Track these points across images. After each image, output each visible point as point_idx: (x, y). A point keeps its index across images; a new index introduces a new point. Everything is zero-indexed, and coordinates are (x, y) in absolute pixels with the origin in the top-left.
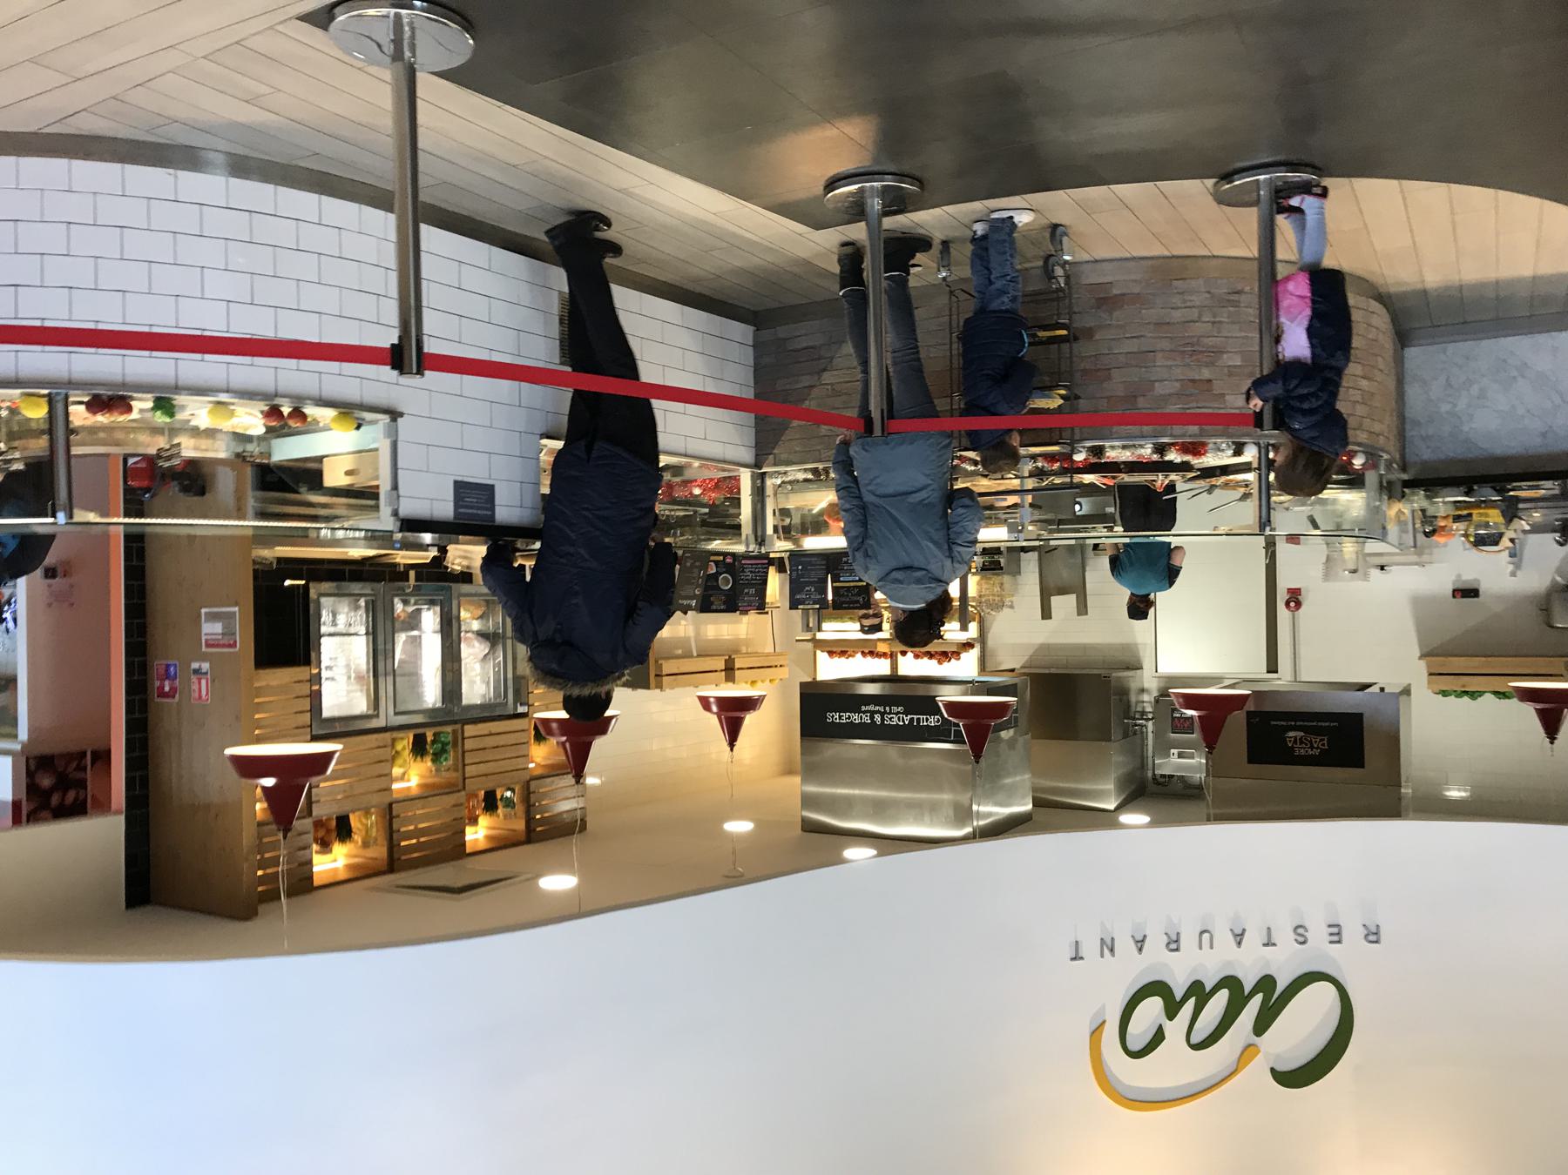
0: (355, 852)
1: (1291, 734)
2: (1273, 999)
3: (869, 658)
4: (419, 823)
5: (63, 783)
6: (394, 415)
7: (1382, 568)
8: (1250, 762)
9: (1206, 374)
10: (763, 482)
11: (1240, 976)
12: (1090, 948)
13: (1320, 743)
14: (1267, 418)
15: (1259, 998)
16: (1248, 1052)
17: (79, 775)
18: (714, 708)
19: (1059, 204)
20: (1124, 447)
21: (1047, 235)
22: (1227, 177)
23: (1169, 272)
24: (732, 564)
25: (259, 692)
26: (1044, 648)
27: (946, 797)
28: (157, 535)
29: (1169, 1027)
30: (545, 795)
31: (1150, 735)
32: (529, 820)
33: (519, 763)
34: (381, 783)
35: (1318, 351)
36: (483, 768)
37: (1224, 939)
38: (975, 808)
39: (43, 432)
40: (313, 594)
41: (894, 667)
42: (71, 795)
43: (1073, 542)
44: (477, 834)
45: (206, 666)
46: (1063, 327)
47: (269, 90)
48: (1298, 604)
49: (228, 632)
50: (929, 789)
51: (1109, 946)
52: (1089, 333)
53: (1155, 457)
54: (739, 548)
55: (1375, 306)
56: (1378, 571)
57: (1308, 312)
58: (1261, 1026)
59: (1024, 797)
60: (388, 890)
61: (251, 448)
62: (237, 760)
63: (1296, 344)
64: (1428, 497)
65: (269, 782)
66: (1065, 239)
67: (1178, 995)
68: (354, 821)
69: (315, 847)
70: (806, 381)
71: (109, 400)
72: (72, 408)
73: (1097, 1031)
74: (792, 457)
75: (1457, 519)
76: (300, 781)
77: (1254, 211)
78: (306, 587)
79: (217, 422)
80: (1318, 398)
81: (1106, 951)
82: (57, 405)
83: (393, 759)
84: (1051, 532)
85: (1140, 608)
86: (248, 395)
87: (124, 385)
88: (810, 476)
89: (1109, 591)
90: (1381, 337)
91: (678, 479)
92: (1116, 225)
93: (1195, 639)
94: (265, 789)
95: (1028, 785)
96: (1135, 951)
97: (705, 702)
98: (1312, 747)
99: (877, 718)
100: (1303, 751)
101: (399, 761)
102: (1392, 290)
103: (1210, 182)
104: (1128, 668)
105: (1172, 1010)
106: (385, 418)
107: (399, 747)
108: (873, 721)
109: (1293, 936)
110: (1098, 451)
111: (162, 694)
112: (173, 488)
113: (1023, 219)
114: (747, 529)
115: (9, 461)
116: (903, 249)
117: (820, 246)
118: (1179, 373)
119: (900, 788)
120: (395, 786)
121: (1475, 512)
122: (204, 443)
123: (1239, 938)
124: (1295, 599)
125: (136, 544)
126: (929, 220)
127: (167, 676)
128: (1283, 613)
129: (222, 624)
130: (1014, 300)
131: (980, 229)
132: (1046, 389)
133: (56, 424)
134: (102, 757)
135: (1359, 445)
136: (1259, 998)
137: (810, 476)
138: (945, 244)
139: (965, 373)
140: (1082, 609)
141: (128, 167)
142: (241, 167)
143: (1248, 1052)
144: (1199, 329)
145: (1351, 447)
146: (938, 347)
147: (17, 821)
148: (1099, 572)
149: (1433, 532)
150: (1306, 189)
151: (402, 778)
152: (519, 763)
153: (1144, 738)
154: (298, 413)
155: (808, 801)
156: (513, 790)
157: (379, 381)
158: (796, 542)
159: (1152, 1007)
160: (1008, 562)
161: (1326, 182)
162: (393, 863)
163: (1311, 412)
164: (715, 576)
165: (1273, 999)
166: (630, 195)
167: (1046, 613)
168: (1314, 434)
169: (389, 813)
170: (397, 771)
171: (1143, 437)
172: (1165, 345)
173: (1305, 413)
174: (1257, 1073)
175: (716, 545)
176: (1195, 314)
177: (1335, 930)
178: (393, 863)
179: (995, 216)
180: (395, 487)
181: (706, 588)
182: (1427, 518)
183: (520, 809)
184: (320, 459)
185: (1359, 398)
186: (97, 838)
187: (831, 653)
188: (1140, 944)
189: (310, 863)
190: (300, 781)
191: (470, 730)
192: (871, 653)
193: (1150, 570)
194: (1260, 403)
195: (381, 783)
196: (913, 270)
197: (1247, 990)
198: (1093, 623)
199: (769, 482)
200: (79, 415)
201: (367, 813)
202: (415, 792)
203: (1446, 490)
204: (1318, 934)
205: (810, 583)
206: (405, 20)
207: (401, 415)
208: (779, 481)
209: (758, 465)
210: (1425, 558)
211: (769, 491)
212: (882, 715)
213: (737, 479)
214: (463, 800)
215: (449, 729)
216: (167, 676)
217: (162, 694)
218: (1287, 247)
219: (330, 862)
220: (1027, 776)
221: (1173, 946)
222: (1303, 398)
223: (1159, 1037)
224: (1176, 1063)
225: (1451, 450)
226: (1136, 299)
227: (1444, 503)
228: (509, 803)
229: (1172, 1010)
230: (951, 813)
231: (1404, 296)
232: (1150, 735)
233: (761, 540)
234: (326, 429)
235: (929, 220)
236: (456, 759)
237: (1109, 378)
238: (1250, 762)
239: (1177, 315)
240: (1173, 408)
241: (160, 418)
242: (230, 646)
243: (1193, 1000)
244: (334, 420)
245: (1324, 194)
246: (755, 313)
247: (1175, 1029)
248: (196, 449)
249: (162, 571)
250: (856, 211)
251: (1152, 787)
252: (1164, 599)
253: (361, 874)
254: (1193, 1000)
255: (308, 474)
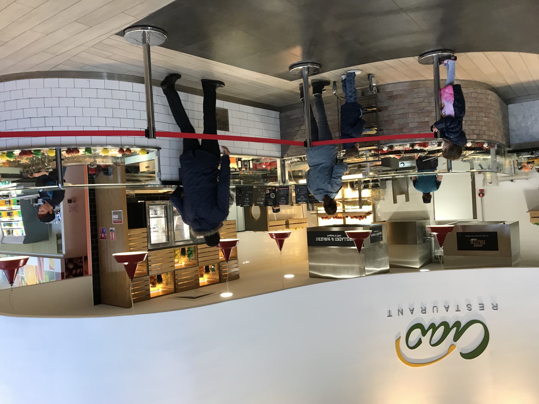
0: (164, 287)
1: (472, 240)
2: (460, 329)
3: (336, 219)
4: (184, 277)
5: (76, 267)
6: (159, 149)
7: (512, 181)
8: (458, 250)
9: (427, 119)
10: (284, 162)
11: (448, 321)
12: (394, 313)
13: (482, 243)
14: (439, 135)
15: (455, 329)
16: (452, 347)
17: (80, 264)
18: (274, 237)
19: (370, 67)
20: (400, 145)
21: (367, 77)
22: (421, 55)
23: (415, 85)
24: (273, 190)
25: (130, 236)
26: (396, 213)
27: (356, 265)
28: (99, 189)
29: (423, 339)
30: (225, 267)
31: (433, 242)
32: (220, 275)
33: (216, 257)
34: (171, 264)
35: (457, 112)
36: (204, 259)
37: (442, 309)
38: (366, 268)
39: (54, 160)
40: (147, 206)
41: (344, 221)
42: (79, 271)
43: (403, 176)
44: (204, 280)
45: (114, 229)
46: (374, 107)
47: (111, 54)
48: (483, 195)
49: (120, 218)
50: (351, 263)
51: (401, 312)
52: (386, 108)
53: (411, 148)
54: (277, 185)
55: (489, 92)
56: (511, 182)
57: (453, 99)
58: (456, 338)
59: (386, 264)
60: (172, 298)
61: (119, 161)
62: (117, 257)
63: (449, 110)
64: (518, 156)
65: (126, 263)
66: (373, 79)
67: (426, 328)
68: (163, 276)
69: (151, 285)
70: (296, 129)
71: (73, 150)
72: (62, 153)
73: (398, 340)
74: (293, 154)
75: (528, 163)
76: (135, 263)
77: (432, 65)
78: (145, 202)
79: (108, 154)
80: (458, 127)
81: (400, 313)
82: (58, 152)
83: (175, 256)
84: (379, 174)
85: (427, 199)
86: (114, 145)
87: (76, 145)
88: (299, 160)
89: (416, 194)
90: (493, 103)
91: (258, 163)
92: (394, 72)
93: (448, 208)
94: (125, 265)
95: (387, 260)
96: (410, 313)
97: (271, 235)
98: (480, 244)
99: (333, 239)
100: (480, 244)
101: (177, 257)
102: (497, 86)
103: (417, 57)
104: (424, 219)
105: (424, 333)
106: (156, 150)
107: (176, 252)
108: (331, 240)
109: (467, 308)
110: (391, 147)
111: (102, 238)
112: (102, 174)
113: (358, 73)
114: (279, 178)
115: (48, 169)
116: (319, 86)
117: (294, 85)
118: (417, 120)
119: (341, 263)
120: (176, 265)
121: (535, 160)
122: (105, 160)
123: (447, 309)
124: (482, 193)
125: (92, 192)
126: (326, 75)
127: (103, 232)
128: (478, 198)
129: (118, 216)
130: (355, 99)
131: (344, 77)
132: (370, 128)
133: (58, 158)
134: (86, 258)
135: (485, 140)
136: (455, 329)
137: (299, 160)
138: (335, 82)
139: (341, 124)
140: (407, 199)
141: (75, 79)
142: (111, 76)
143: (452, 347)
144: (423, 104)
145: (360, 153)
146: (333, 117)
147: (63, 278)
148: (411, 188)
149: (521, 168)
150: (449, 57)
151: (178, 262)
152: (216, 257)
153: (431, 242)
154: (128, 150)
155: (311, 268)
156: (214, 266)
157: (143, 140)
158: (297, 181)
159: (417, 332)
160: (381, 184)
161: (455, 55)
162: (176, 290)
163: (456, 132)
164: (269, 194)
165: (460, 329)
166: (229, 75)
167: (395, 201)
168: (457, 140)
169: (174, 273)
170: (176, 260)
171: (405, 142)
172: (412, 111)
173: (454, 133)
174: (455, 354)
175: (270, 184)
176: (422, 99)
177: (482, 306)
178: (176, 290)
179: (349, 72)
180: (160, 171)
181: (266, 198)
182: (519, 164)
183: (217, 272)
184: (139, 163)
185: (484, 124)
186: (85, 283)
187: (322, 218)
188: (412, 311)
189: (149, 290)
190: (135, 263)
191: (199, 246)
192: (336, 217)
193: (429, 185)
194: (437, 130)
195: (171, 264)
196: (323, 92)
197: (451, 326)
198: (412, 204)
199: (286, 162)
200: (64, 153)
201: (167, 273)
202: (183, 267)
203: (525, 153)
204: (475, 307)
205: (302, 195)
206: (146, 33)
207: (161, 149)
208: (289, 162)
209: (282, 157)
210: (528, 177)
211: (286, 165)
212: (334, 238)
213: (276, 162)
214: (198, 269)
215: (192, 246)
216: (103, 232)
217: (102, 238)
218: (444, 76)
219: (156, 290)
220: (387, 258)
221: (424, 312)
222: (452, 128)
223: (420, 342)
224: (426, 351)
225: (527, 139)
226: (401, 96)
227: (524, 158)
228: (213, 270)
229: (424, 333)
230: (358, 270)
231: (501, 88)
232: (433, 242)
233: (284, 181)
234: (139, 154)
235: (326, 75)
236: (195, 256)
237: (393, 123)
238: (458, 250)
239: (416, 101)
240: (416, 132)
241: (88, 154)
242: (121, 222)
243: (431, 330)
244: (140, 151)
245: (455, 59)
246: (280, 108)
247: (426, 339)
248: (103, 162)
249: (100, 200)
250: (301, 75)
251: (435, 260)
252: (436, 194)
253: (166, 294)
254: (431, 330)
255: (135, 168)
